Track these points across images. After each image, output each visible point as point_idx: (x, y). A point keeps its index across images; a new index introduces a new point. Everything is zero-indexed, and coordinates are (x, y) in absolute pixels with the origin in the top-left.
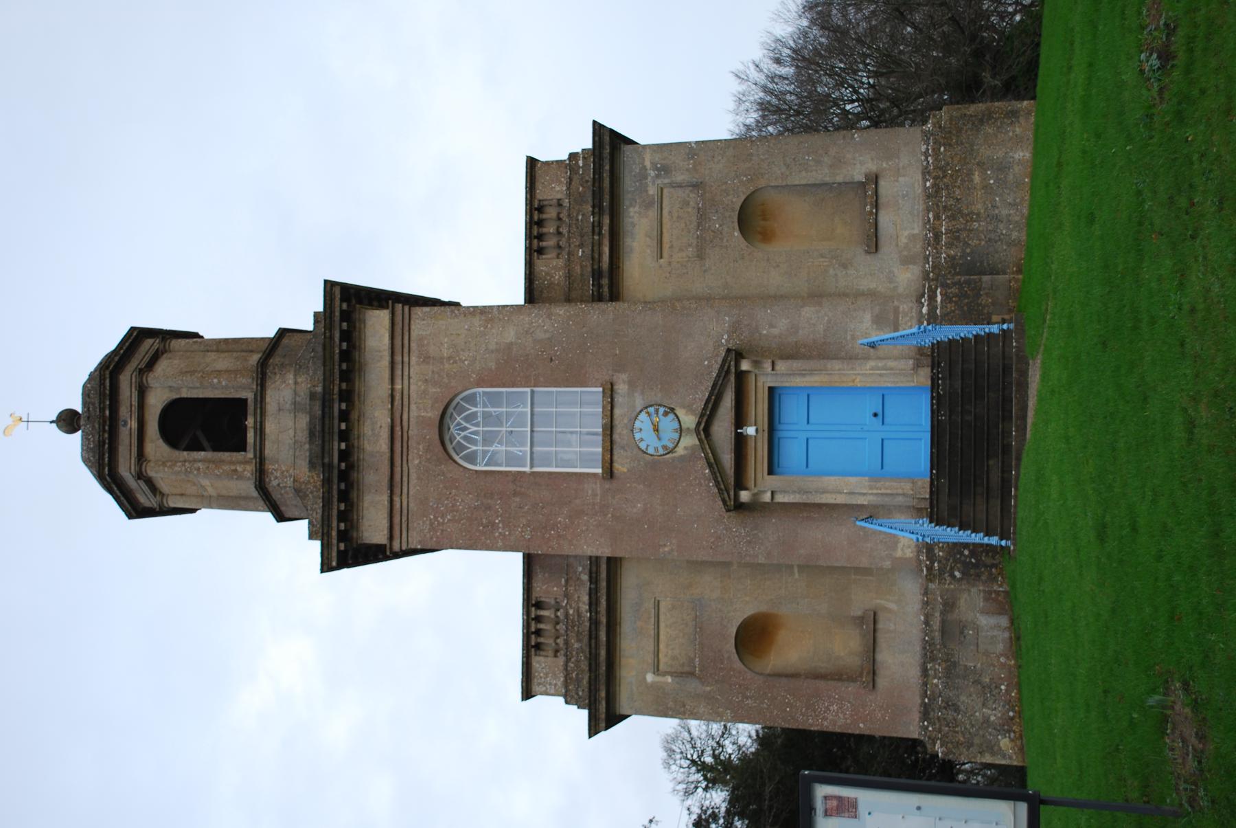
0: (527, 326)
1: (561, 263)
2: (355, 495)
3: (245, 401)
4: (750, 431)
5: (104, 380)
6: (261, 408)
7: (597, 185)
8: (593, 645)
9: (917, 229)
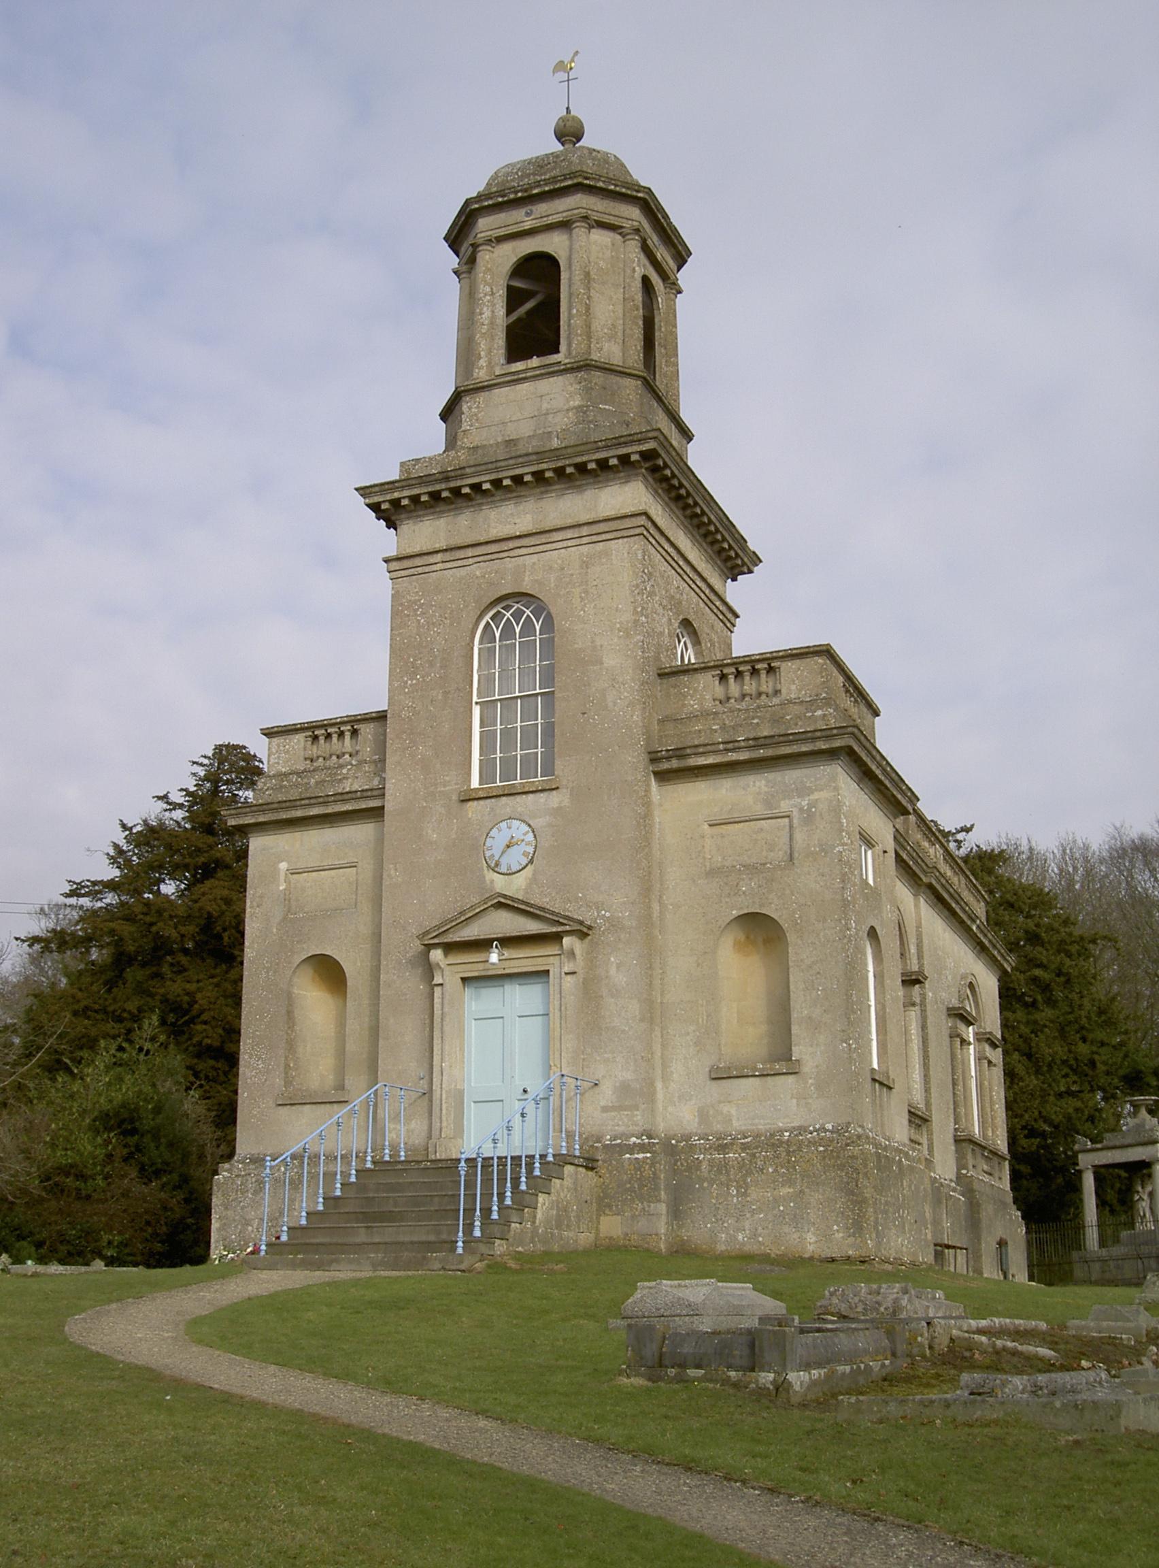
0: (621, 680)
1: (709, 704)
2: (442, 508)
3: (557, 351)
4: (494, 957)
5: (571, 178)
6: (542, 375)
7: (782, 739)
8: (303, 802)
9: (738, 1125)
